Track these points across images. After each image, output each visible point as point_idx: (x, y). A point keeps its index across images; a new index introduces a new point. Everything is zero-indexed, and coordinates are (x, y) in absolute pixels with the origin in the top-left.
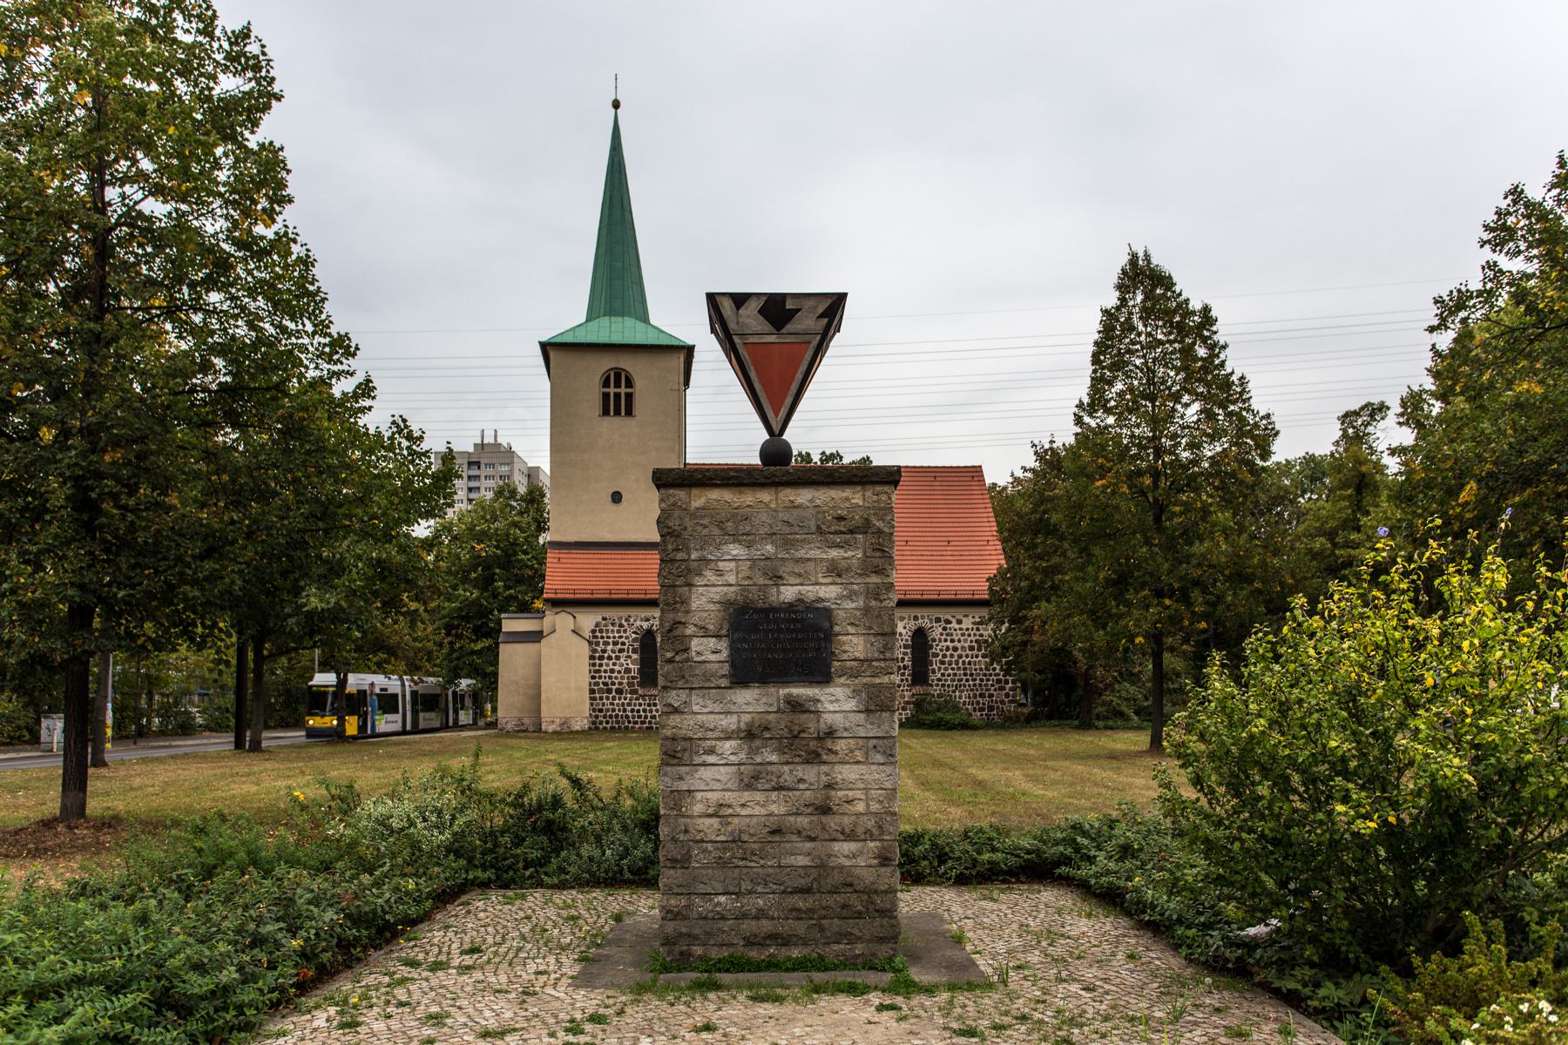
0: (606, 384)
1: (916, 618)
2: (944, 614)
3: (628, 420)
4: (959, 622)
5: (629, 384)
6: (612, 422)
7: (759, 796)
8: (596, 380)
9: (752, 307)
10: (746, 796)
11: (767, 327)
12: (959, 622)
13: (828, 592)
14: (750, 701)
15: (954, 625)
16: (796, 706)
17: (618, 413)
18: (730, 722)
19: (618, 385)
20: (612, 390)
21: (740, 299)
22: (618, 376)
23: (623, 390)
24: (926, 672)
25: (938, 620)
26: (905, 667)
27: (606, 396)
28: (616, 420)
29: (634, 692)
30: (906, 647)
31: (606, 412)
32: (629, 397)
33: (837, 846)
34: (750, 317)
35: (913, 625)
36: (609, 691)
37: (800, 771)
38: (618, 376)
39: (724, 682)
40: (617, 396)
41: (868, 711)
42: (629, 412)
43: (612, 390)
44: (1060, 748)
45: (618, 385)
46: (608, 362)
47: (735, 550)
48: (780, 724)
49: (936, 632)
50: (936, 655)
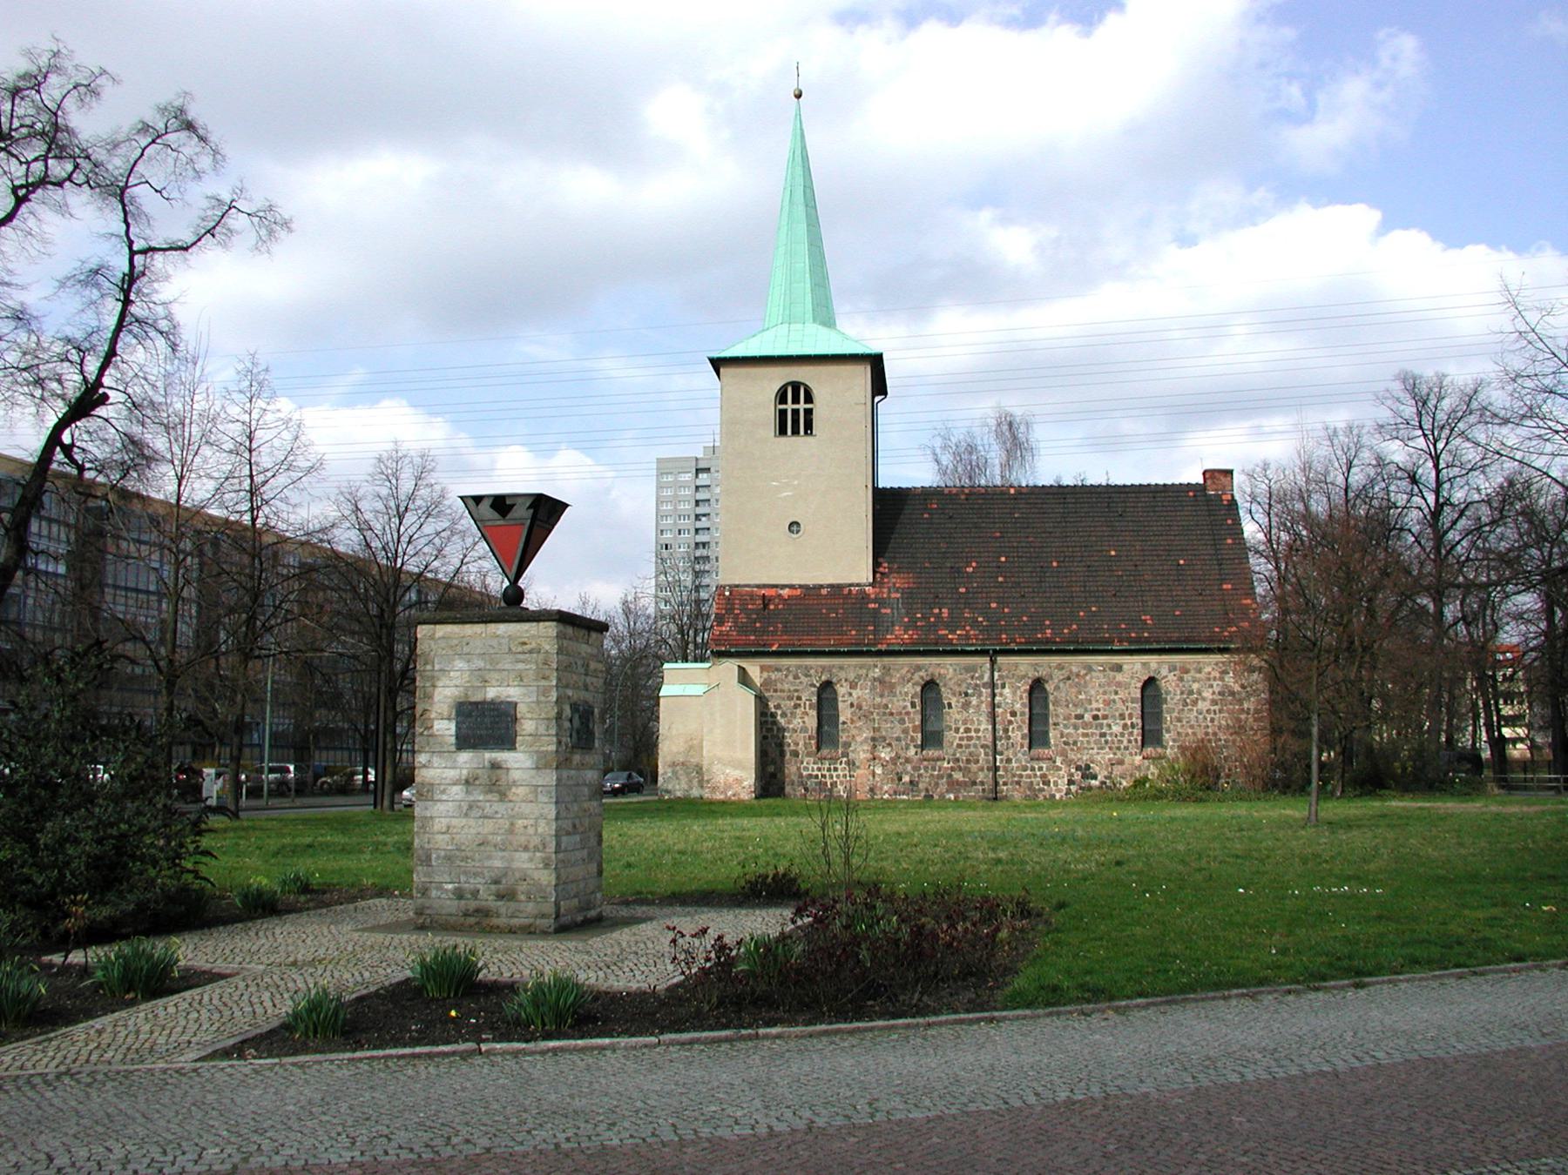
0: (782, 398)
3: (809, 439)
5: (809, 399)
6: (789, 441)
7: (472, 822)
9: (485, 505)
10: (464, 821)
11: (496, 515)
13: (512, 693)
14: (466, 759)
16: (495, 766)
17: (796, 432)
18: (452, 774)
19: (796, 400)
20: (790, 406)
21: (478, 499)
23: (802, 406)
26: (1133, 726)
27: (783, 413)
28: (795, 438)
32: (809, 412)
33: (517, 855)
34: (485, 507)
37: (496, 806)
39: (453, 748)
40: (796, 412)
41: (537, 768)
42: (809, 426)
43: (802, 406)
44: (1070, 817)
45: (796, 400)
46: (779, 377)
47: (460, 664)
50: (1170, 711)
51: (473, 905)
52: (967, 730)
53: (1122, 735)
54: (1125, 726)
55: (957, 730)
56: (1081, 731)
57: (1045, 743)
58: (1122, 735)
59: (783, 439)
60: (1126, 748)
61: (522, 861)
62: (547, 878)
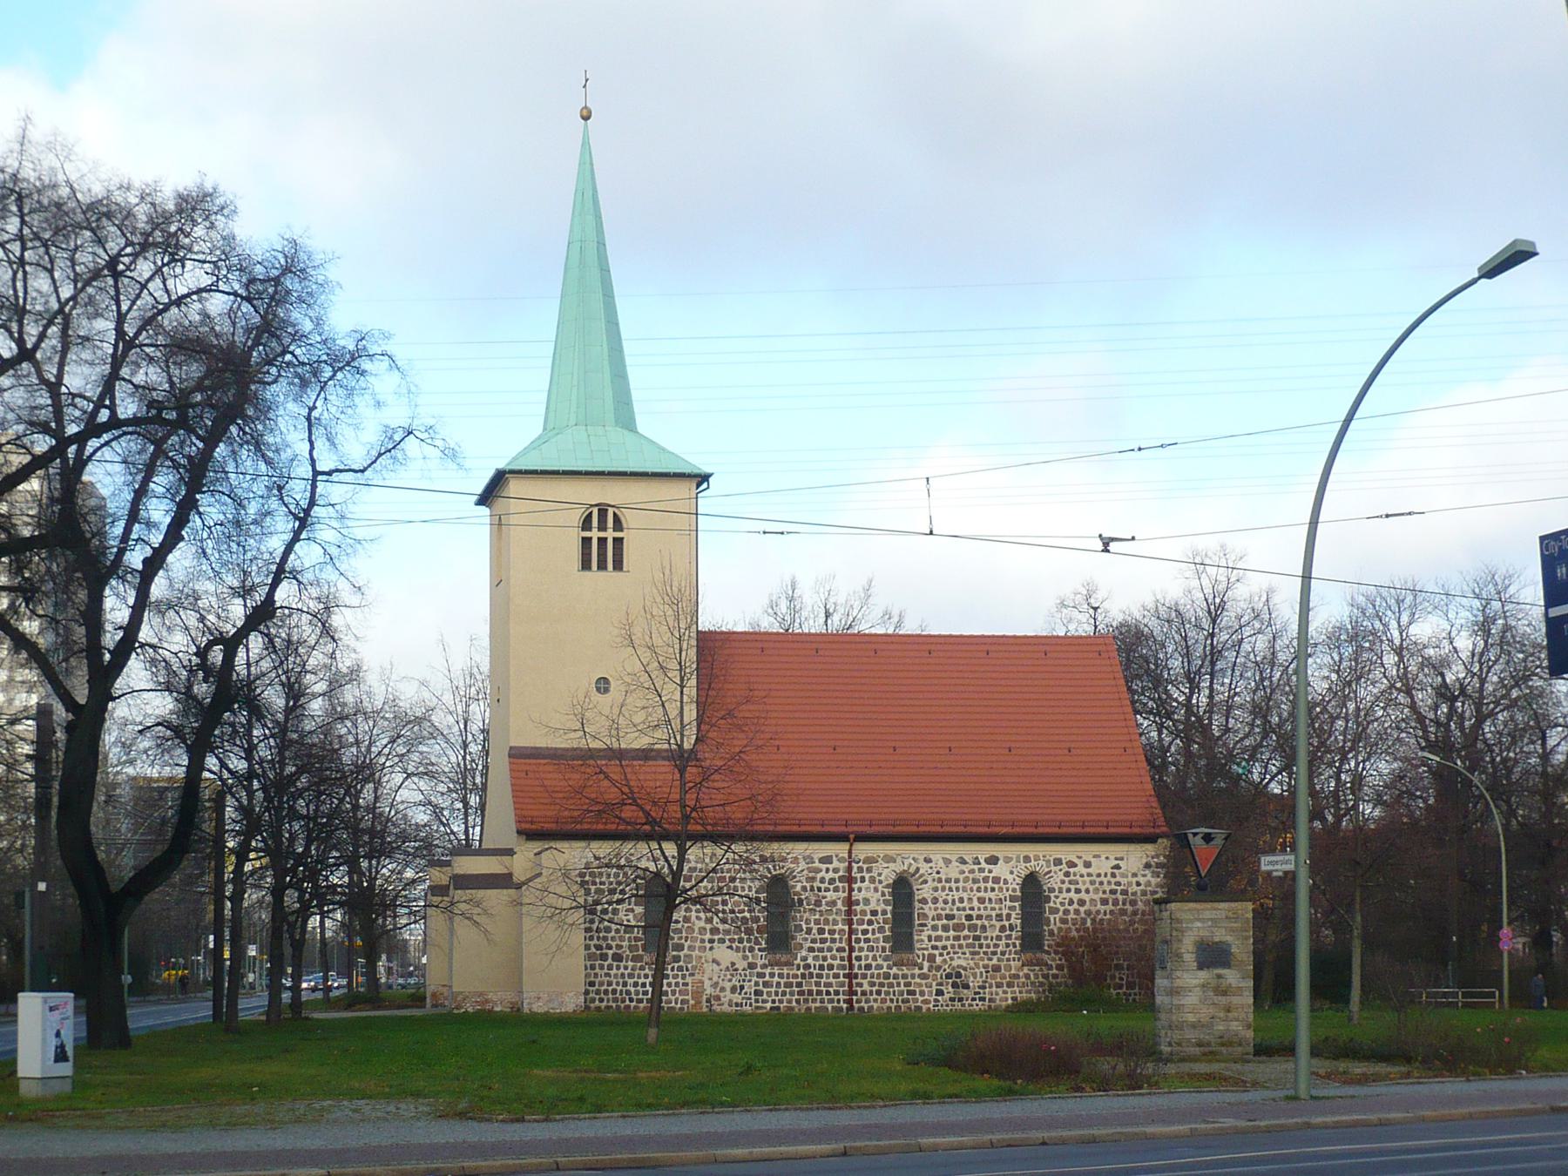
0: (586, 524)
1: (1027, 859)
2: (1066, 852)
3: (610, 574)
4: (1088, 865)
6: (596, 578)
8: (577, 516)
12: (1088, 865)
13: (1229, 939)
14: (1204, 975)
15: (1081, 869)
16: (1219, 976)
17: (602, 566)
19: (602, 528)
20: (595, 534)
22: (603, 513)
23: (595, 534)
24: (911, 915)
25: (1058, 862)
26: (1011, 928)
27: (586, 542)
28: (602, 574)
29: (636, 959)
30: (1012, 899)
31: (586, 565)
32: (618, 542)
35: (1023, 870)
36: (604, 957)
38: (603, 513)
42: (618, 565)
43: (610, 534)
46: (594, 493)
48: (1214, 982)
49: (1055, 880)
51: (1207, 1049)
52: (821, 931)
53: (999, 938)
54: (1003, 929)
55: (809, 931)
56: (952, 933)
57: (910, 947)
58: (999, 938)
59: (587, 573)
60: (1003, 953)
61: (1235, 1026)
62: (1250, 1034)
